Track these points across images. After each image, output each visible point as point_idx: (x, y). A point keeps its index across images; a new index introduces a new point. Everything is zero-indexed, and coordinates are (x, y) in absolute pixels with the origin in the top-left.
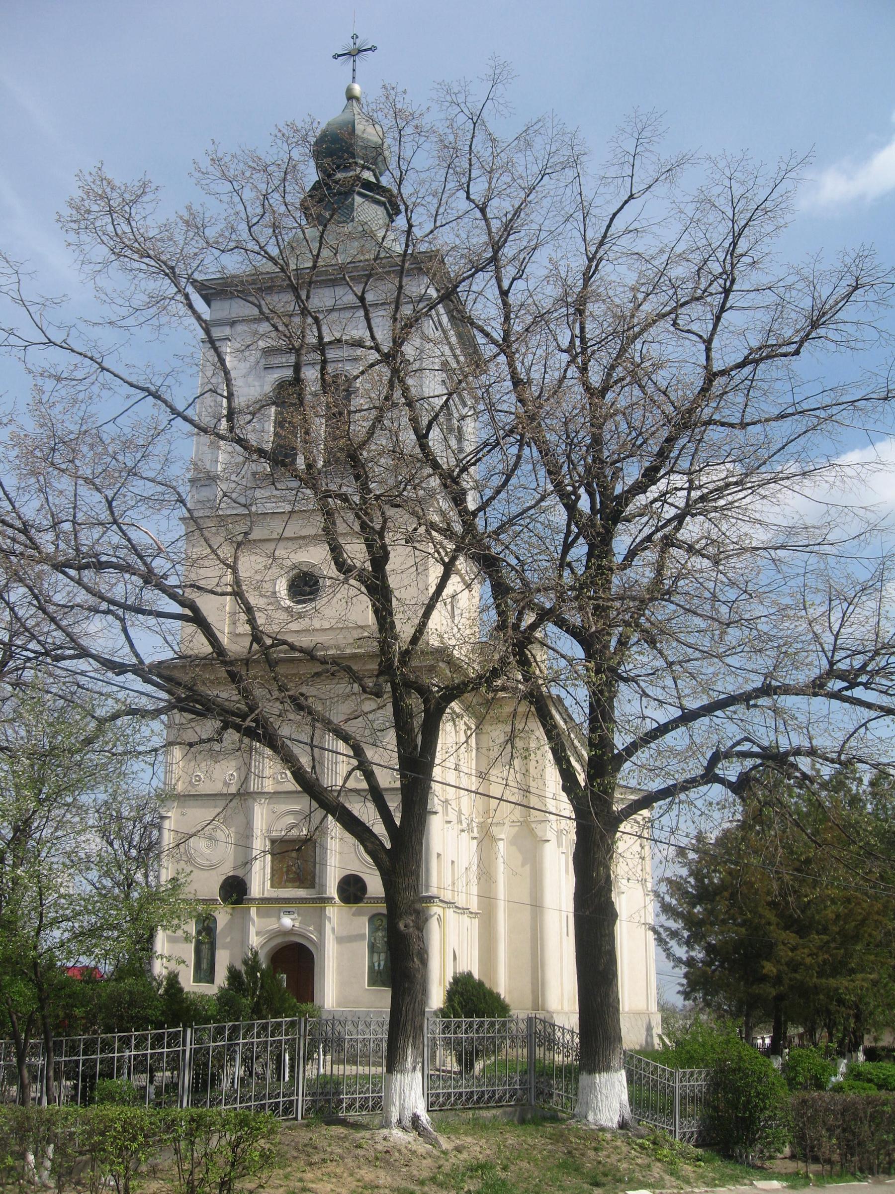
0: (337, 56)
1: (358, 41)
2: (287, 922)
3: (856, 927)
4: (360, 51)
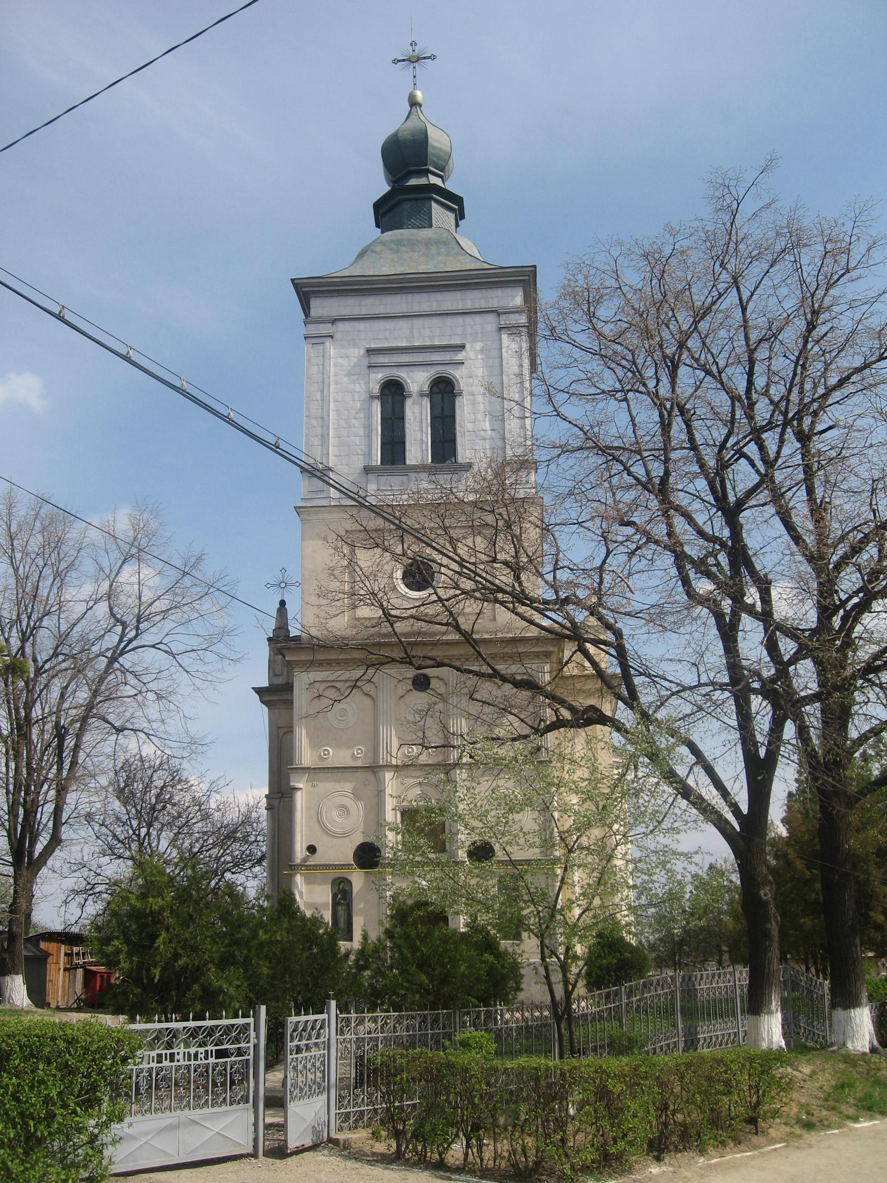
0: (396, 61)
1: (417, 49)
4: (419, 59)
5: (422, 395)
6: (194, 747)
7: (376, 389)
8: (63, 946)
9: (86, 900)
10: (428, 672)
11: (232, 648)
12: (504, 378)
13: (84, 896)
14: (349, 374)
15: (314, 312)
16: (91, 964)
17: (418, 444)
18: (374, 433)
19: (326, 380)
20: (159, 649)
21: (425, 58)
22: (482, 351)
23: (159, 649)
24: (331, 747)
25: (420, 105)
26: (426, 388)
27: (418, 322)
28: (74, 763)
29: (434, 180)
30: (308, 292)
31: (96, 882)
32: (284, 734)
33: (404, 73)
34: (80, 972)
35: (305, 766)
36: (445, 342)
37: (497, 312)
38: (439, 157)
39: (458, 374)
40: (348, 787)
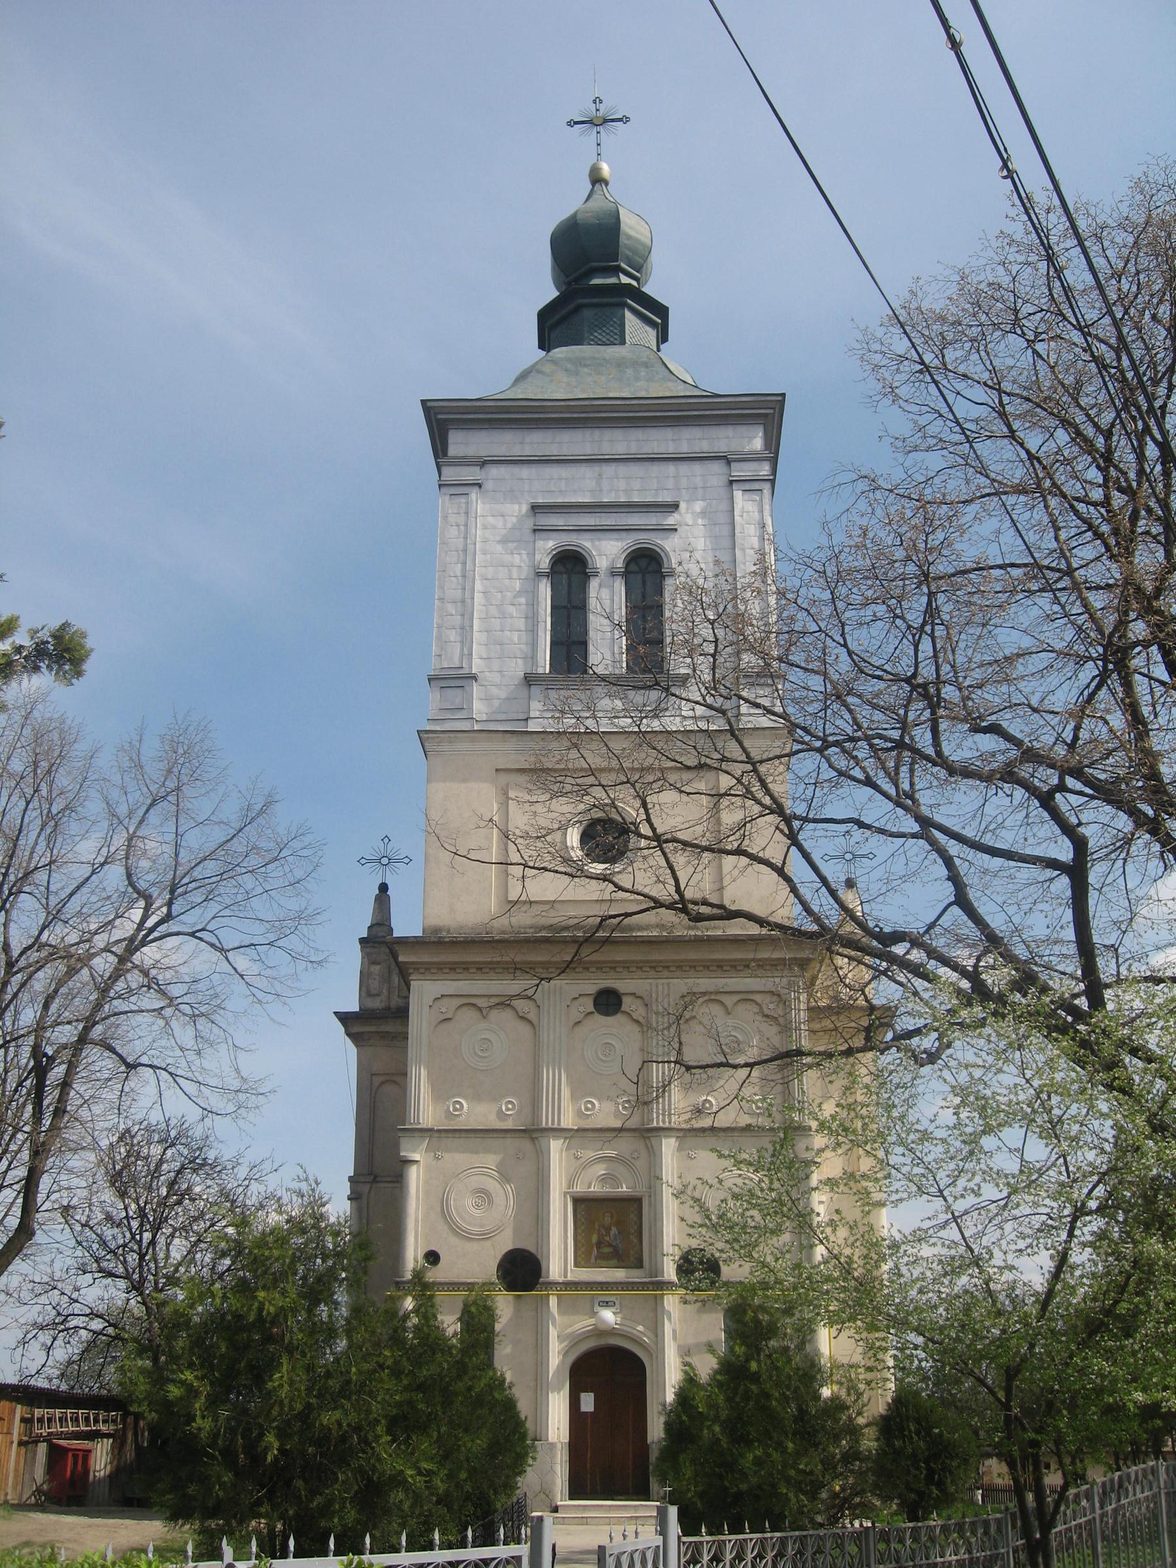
1: (602, 107)
2: (608, 1316)
3: (300, 1497)
4: (606, 121)
5: (613, 574)
6: (242, 1097)
7: (545, 563)
8: (19, 1406)
9: (55, 1339)
10: (621, 985)
11: (312, 944)
12: (737, 552)
13: (52, 1332)
14: (504, 541)
15: (453, 451)
16: (61, 1436)
17: (607, 648)
18: (541, 625)
19: (470, 547)
20: (200, 939)
21: (613, 120)
22: (703, 513)
23: (200, 939)
24: (466, 1098)
25: (607, 184)
26: (620, 564)
27: (609, 470)
28: (59, 1112)
29: (625, 280)
30: (446, 420)
31: (70, 1311)
32: (383, 1083)
33: (585, 139)
34: (42, 1448)
35: (425, 1126)
36: (649, 498)
37: (727, 460)
38: (635, 252)
39: (670, 546)
40: (491, 1161)
